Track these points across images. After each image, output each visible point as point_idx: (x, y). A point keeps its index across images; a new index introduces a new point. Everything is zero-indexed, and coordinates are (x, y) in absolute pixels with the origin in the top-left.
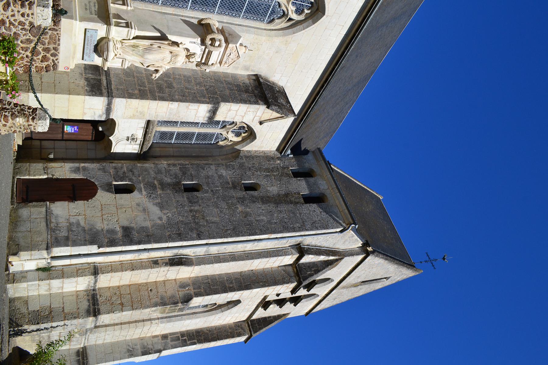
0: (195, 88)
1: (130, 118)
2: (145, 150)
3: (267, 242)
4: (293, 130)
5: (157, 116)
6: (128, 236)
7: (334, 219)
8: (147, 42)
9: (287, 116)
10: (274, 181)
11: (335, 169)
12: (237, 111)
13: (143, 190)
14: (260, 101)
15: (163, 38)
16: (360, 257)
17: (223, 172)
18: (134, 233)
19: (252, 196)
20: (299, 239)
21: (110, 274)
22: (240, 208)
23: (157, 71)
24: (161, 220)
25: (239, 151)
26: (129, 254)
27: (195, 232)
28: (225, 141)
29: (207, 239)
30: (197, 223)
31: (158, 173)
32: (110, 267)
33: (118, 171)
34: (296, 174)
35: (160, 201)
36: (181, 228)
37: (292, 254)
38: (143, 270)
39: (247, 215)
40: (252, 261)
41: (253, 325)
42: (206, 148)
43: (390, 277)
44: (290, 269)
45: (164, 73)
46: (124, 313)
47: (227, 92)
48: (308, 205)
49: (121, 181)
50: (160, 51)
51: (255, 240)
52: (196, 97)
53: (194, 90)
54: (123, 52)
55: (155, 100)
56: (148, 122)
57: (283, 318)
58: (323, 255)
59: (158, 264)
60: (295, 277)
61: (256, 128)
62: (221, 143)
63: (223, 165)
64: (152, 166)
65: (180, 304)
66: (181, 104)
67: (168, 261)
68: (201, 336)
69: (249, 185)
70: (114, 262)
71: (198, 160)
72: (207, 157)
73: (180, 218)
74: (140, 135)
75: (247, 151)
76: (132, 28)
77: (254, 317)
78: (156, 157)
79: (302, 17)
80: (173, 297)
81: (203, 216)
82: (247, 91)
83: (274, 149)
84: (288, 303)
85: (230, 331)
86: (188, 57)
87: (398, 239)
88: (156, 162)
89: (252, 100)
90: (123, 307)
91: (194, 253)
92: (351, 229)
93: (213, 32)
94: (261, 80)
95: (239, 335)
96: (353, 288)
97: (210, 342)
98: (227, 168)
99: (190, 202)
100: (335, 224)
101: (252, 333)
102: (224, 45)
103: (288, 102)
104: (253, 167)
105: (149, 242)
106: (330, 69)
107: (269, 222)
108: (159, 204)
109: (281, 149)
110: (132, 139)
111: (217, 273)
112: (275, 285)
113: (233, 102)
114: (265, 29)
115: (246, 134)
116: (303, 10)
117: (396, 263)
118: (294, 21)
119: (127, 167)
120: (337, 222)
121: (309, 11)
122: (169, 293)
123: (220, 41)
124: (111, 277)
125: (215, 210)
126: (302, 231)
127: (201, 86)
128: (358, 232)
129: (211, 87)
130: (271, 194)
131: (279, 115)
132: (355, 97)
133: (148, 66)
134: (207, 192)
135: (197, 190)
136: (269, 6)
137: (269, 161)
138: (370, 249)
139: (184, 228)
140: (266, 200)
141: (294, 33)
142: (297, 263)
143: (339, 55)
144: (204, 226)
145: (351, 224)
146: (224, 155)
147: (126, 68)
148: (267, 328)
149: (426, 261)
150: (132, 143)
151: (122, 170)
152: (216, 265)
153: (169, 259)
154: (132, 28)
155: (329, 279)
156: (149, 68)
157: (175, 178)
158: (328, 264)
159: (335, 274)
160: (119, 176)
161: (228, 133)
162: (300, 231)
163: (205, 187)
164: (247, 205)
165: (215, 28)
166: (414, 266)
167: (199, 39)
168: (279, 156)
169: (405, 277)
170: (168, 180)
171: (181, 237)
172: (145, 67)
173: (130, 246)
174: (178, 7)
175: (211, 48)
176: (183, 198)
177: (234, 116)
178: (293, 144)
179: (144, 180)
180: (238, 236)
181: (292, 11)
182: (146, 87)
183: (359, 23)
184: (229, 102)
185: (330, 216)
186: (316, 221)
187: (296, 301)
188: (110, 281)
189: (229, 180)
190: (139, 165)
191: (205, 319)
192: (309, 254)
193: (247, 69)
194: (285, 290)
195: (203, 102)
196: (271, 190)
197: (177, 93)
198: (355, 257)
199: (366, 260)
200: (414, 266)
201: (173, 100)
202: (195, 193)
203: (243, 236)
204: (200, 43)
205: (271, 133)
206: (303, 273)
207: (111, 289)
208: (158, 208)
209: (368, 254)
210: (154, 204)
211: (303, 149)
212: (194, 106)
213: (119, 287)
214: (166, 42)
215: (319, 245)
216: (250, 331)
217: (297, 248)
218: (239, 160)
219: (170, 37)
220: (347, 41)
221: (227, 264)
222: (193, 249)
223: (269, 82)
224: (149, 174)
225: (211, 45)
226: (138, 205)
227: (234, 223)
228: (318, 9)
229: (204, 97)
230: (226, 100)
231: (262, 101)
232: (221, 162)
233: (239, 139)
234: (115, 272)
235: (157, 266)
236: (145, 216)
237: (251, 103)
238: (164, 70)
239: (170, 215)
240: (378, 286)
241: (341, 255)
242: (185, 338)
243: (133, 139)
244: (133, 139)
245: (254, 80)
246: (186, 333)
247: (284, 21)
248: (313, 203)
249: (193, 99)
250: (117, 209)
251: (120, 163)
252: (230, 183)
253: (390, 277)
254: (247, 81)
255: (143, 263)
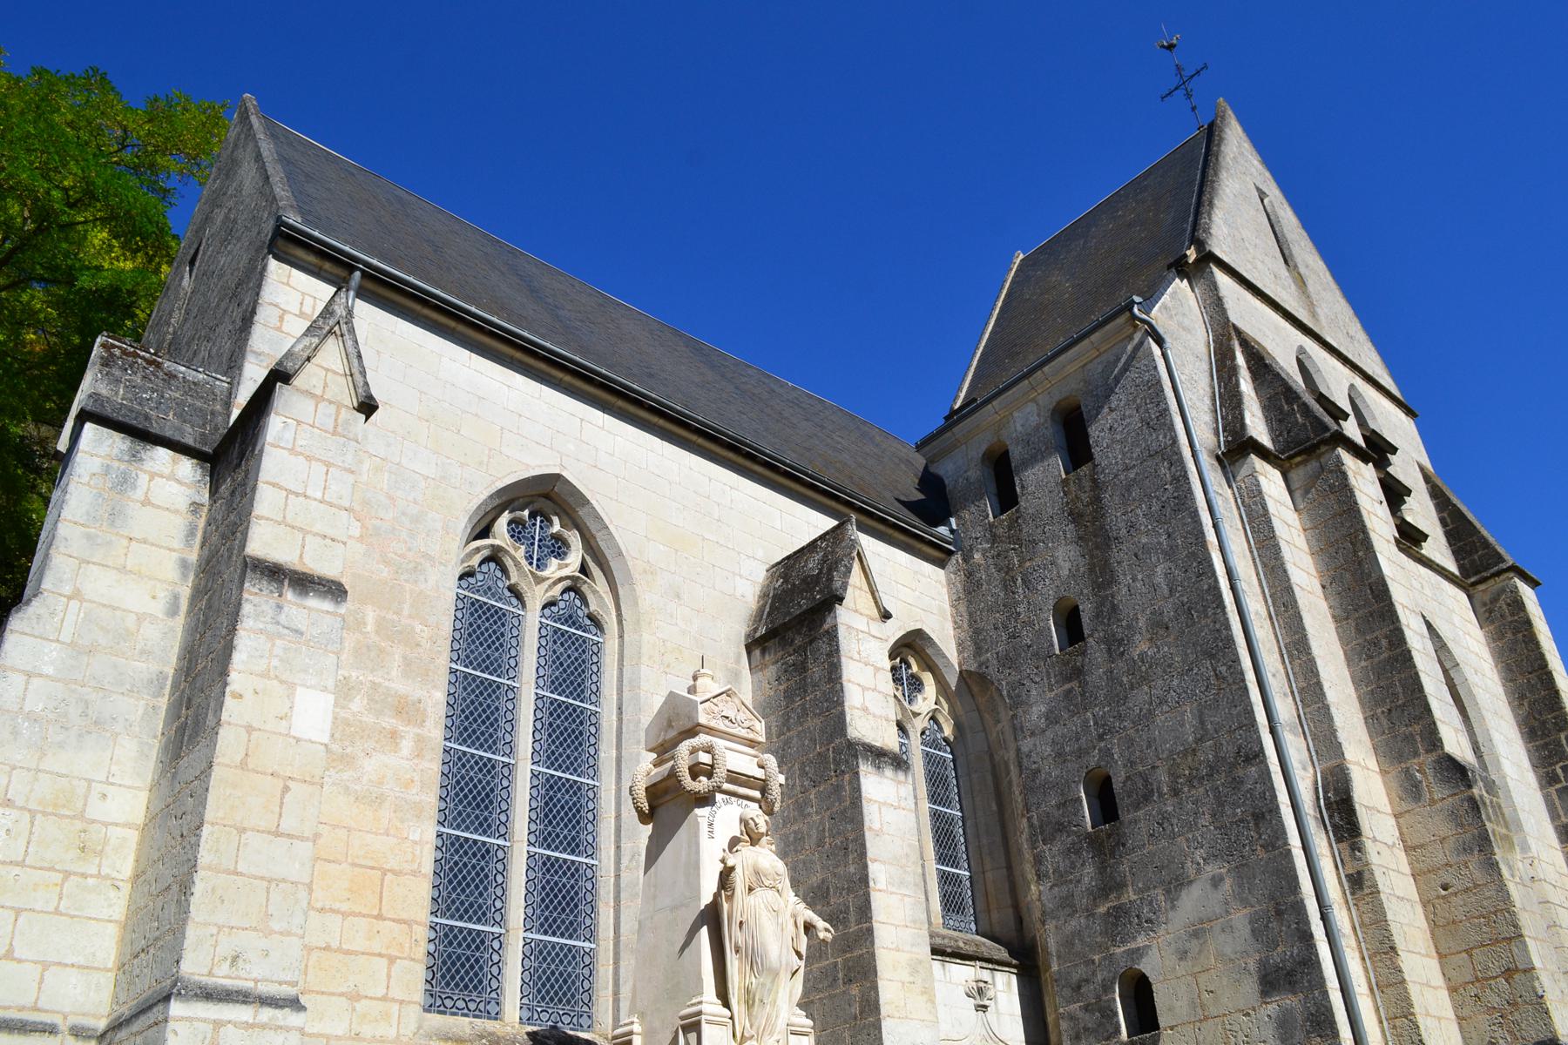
0: (816, 818)
1: (933, 1002)
2: (1003, 954)
3: (1232, 551)
4: (881, 527)
5: (914, 922)
6: (1290, 974)
7: (1125, 369)
8: (733, 963)
9: (854, 543)
10: (1038, 561)
11: (962, 395)
12: (864, 689)
13: (1133, 945)
14: (826, 627)
15: (712, 917)
16: (1222, 278)
17: (1036, 713)
18: (1276, 956)
19: (1097, 616)
20: (1207, 461)
21: (1421, 1020)
22: (1141, 646)
23: (809, 928)
24: (1222, 879)
25: (964, 676)
26: (1343, 962)
27: (1241, 773)
28: (941, 720)
29: (1257, 731)
30: (1213, 770)
31: (1072, 906)
32: (1398, 1022)
33: (1086, 1029)
34: (1007, 498)
35: (1159, 891)
36: (1235, 815)
37: (1253, 475)
38: (1389, 917)
39: (1158, 625)
40: (1297, 590)
41: (1477, 566)
42: (969, 775)
43: (1258, 189)
44: (1298, 475)
45: (811, 905)
46: (1537, 963)
47: (813, 723)
48: (1095, 451)
49: (1116, 1014)
50: (752, 923)
51: (1233, 588)
52: (844, 812)
53: (822, 822)
54: (771, 1034)
55: (870, 931)
56: (936, 951)
57: (1439, 483)
58: (1237, 385)
59: (1359, 873)
60: (1319, 456)
61: (894, 631)
62: (948, 731)
63: (1014, 716)
64: (1050, 925)
65: (1475, 791)
66: (870, 854)
67: (1344, 845)
68: (1544, 723)
69: (1064, 631)
70: (1377, 1010)
71: (1011, 793)
72: (994, 766)
73: (1202, 822)
74: (964, 973)
75: (960, 652)
76: (700, 1013)
77: (1453, 568)
78: (1020, 920)
79: (574, 538)
80: (1453, 816)
81: (1185, 753)
82: (801, 668)
83: (941, 572)
84: (1390, 469)
85: (1509, 635)
86: (754, 840)
87: (1137, 185)
88: (1037, 914)
89: (825, 648)
90: (1517, 970)
91: (1305, 769)
92: (1148, 314)
93: (673, 774)
94: (762, 631)
95: (1518, 605)
96: (1311, 288)
97: (1557, 692)
98: (1022, 703)
99: (1147, 798)
100: (1140, 364)
101: (1504, 566)
102: (702, 739)
103: (812, 546)
104: (1005, 627)
105: (1300, 908)
106: (700, 441)
107: (1170, 554)
108: (1168, 891)
109: (938, 554)
110: (979, 995)
111: (1350, 689)
112: (1359, 511)
113: (841, 703)
114: (621, 637)
115: (912, 661)
116: (553, 536)
117: (1216, 174)
118: (588, 559)
119: (1069, 1002)
120: (1132, 357)
121: (556, 520)
122: (1446, 829)
123: (694, 751)
124: (1428, 1015)
125: (1160, 719)
126: (1179, 453)
127: (807, 803)
128: (1152, 294)
129: (804, 774)
130: (1081, 561)
131: (856, 566)
132: (750, 371)
133: (798, 954)
134: (1107, 753)
135: (1107, 782)
136: (465, 678)
137: (979, 585)
138: (1192, 254)
139: (1235, 805)
140: (1101, 575)
141: (621, 554)
142: (1277, 457)
143: (661, 422)
144: (1217, 747)
145: (1134, 317)
146: (981, 718)
147: (810, 1023)
148: (1478, 525)
149: (1188, 96)
150: (991, 993)
151: (1080, 1014)
152: (1332, 695)
153: (1339, 841)
154: (700, 1013)
155: (1299, 361)
156: (803, 951)
157: (1078, 852)
158: (1261, 365)
159: (1282, 345)
160: (1100, 1024)
161: (916, 715)
162: (1181, 461)
163: (1093, 759)
164: (1129, 627)
165: (655, 771)
166: (1211, 126)
167: (698, 811)
168: (958, 556)
169: (1247, 146)
170: (1088, 873)
171: (1266, 813)
172: (802, 963)
173: (1324, 966)
174: (593, 891)
175: (720, 773)
176: (1137, 821)
177: (881, 696)
178: (922, 519)
179: (1100, 947)
180: (1230, 640)
181: (560, 567)
182: (836, 964)
183: (568, 378)
184: (843, 713)
185: (1117, 380)
186: (1142, 420)
187: (1377, 450)
188: (1439, 1019)
189: (1058, 691)
190: (1055, 968)
191: (1488, 716)
192: (1243, 426)
193: (735, 676)
194: (1363, 480)
195: (857, 789)
196: (1068, 565)
197: (840, 870)
198: (1223, 292)
199: (1226, 259)
200: (1211, 126)
201: (864, 880)
202: (1117, 785)
203: (1228, 627)
204: (708, 809)
205: (902, 591)
206: (1302, 436)
207: (1466, 1012)
208: (1184, 893)
209: (1208, 258)
210: (1173, 907)
211: (921, 496)
212: (873, 816)
213: (1453, 990)
214: (726, 906)
215: (1208, 401)
216: (1498, 574)
217: (1232, 463)
218: (992, 671)
219: (706, 898)
220: (620, 403)
221: (1319, 663)
222: (1295, 773)
223: (761, 610)
224: (1078, 933)
225: (710, 775)
226: (1183, 955)
227: (1192, 657)
228: (547, 496)
229: (838, 789)
230: (840, 724)
231: (823, 621)
232: (1005, 724)
233: (928, 679)
234: (1411, 1006)
235: (1366, 875)
236: (1217, 929)
237: (834, 652)
238: (803, 905)
239: (1199, 855)
240: (1289, 219)
241: (1227, 340)
242: (1559, 771)
243: (980, 991)
244: (980, 991)
245: (763, 653)
246: (1542, 771)
247: (590, 587)
248: (1087, 436)
249: (852, 821)
250: (1206, 1018)
251: (1057, 1026)
252: (1067, 686)
253: (1258, 189)
254: (771, 671)
255: (1367, 921)
